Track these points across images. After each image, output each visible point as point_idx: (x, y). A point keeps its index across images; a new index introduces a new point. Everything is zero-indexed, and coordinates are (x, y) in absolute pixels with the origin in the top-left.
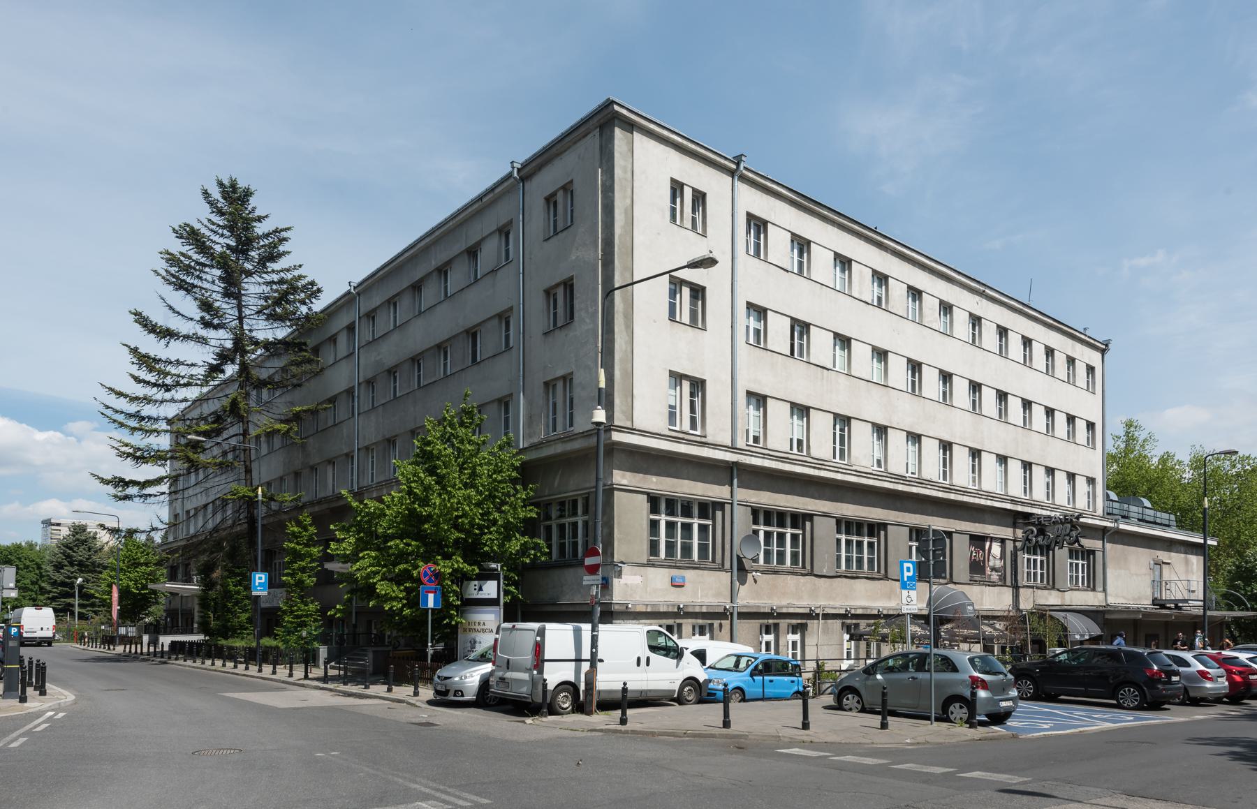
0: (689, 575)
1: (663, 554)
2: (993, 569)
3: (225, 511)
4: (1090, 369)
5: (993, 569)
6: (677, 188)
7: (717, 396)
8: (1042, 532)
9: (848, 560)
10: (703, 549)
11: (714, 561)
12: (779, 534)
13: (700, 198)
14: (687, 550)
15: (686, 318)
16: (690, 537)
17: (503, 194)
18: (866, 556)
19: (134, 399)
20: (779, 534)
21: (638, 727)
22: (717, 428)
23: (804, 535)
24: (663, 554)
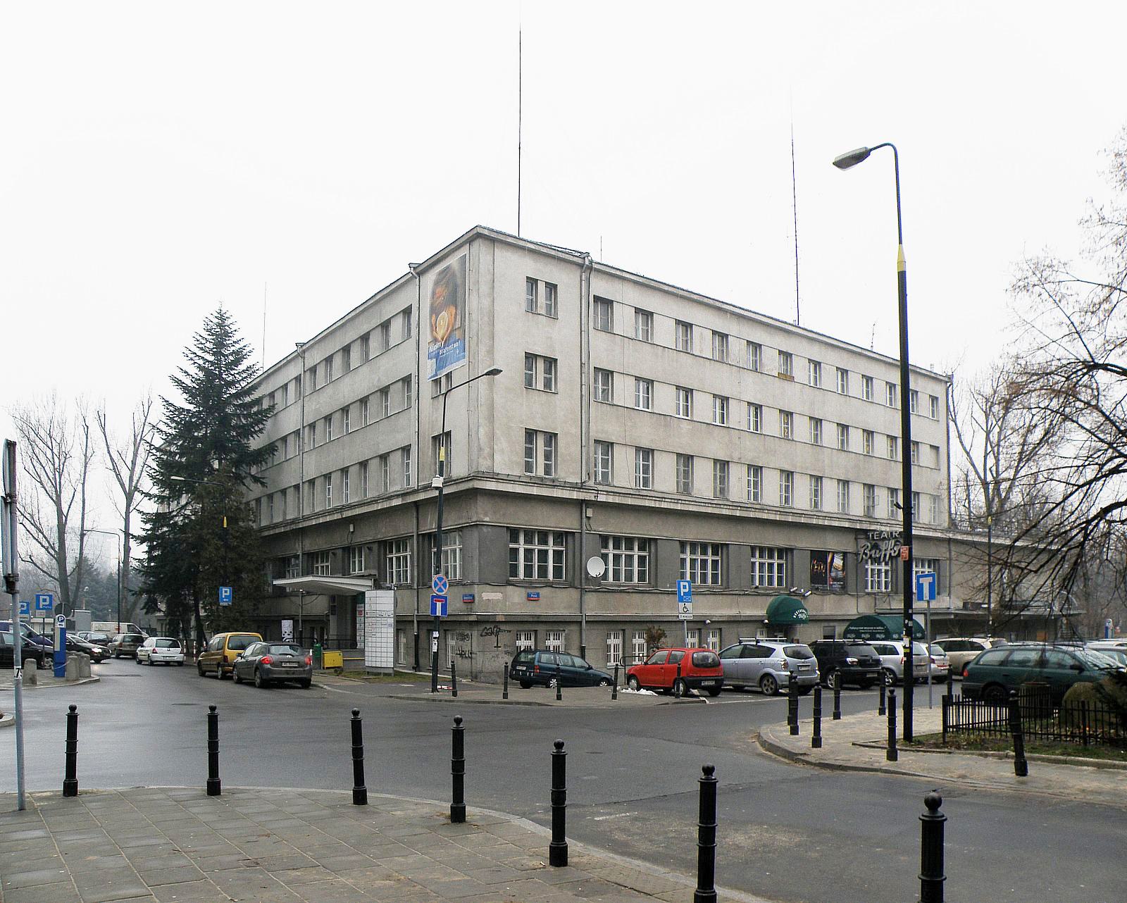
0: (544, 592)
1: (550, 576)
2: (835, 579)
3: (1062, 547)
4: (934, 399)
5: (835, 579)
6: (532, 282)
7: (568, 447)
8: (875, 547)
9: (761, 578)
10: (558, 572)
11: (722, 585)
12: (397, 557)
13: (552, 288)
14: (543, 571)
15: (540, 386)
16: (546, 561)
17: (291, 360)
18: (623, 568)
19: (444, 277)
20: (397, 557)
21: (462, 699)
22: (569, 471)
23: (649, 556)
24: (550, 576)
